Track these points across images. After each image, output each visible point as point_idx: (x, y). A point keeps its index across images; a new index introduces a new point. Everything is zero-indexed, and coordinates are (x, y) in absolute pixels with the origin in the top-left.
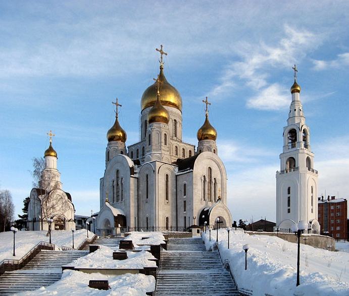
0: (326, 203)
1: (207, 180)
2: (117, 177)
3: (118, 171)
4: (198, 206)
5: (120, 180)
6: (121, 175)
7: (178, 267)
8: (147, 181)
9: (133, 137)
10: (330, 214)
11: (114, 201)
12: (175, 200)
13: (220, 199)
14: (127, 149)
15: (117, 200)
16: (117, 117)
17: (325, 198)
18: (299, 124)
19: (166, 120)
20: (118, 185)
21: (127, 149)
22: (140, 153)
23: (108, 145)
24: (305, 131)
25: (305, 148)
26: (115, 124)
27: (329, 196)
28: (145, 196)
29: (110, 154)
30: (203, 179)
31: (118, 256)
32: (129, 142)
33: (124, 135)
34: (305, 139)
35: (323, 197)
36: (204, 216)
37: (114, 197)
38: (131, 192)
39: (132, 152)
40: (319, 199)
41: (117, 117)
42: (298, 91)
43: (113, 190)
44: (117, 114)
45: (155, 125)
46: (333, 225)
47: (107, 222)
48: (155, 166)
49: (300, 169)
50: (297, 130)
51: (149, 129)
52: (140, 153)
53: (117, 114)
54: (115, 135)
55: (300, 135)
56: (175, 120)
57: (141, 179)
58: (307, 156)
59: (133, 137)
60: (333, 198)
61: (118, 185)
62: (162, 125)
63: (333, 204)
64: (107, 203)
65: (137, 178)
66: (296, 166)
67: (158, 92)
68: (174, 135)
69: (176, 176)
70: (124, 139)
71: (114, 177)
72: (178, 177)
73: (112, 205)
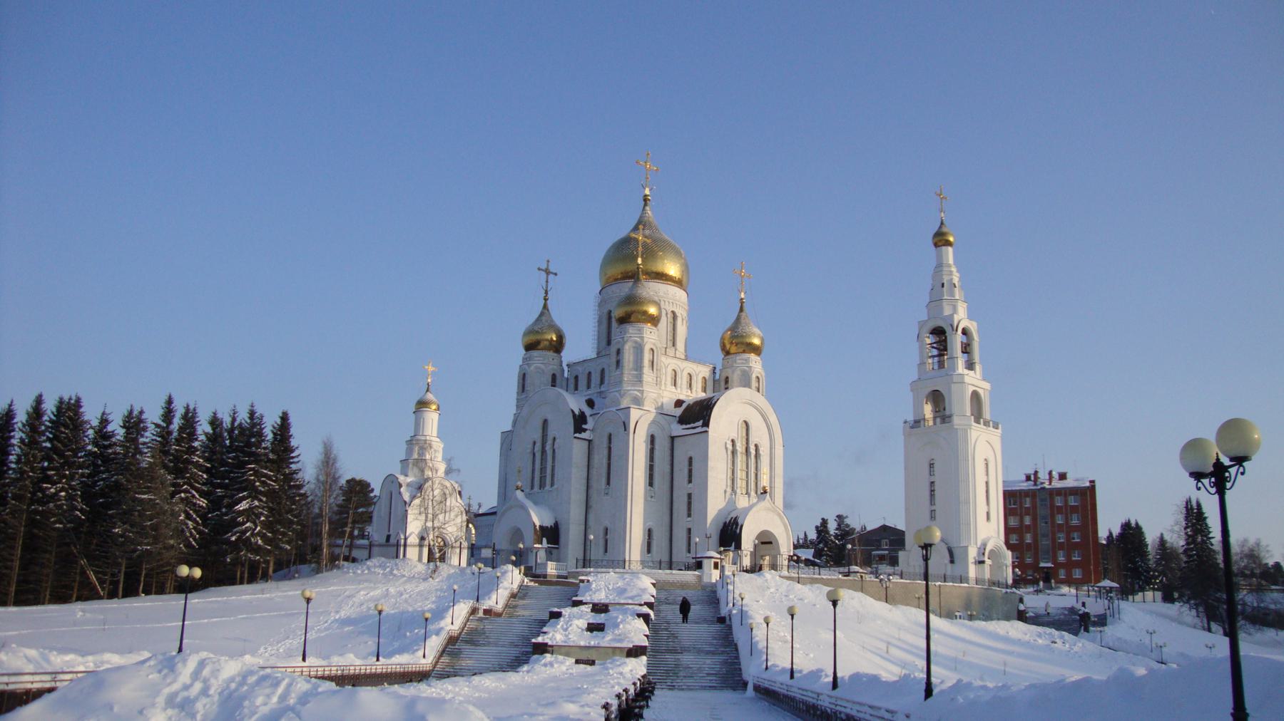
0: (1043, 488)
1: (740, 448)
2: (544, 436)
3: (545, 422)
4: (715, 505)
5: (549, 442)
6: (551, 433)
7: (24, 567)
8: (610, 448)
9: (581, 346)
10: (1053, 516)
11: (532, 487)
12: (668, 512)
13: (765, 492)
14: (566, 369)
15: (542, 486)
16: (546, 300)
17: (1043, 476)
18: (952, 316)
19: (654, 320)
20: (543, 451)
21: (566, 369)
22: (595, 378)
23: (525, 359)
24: (965, 332)
25: (966, 372)
26: (542, 314)
27: (1050, 473)
28: (604, 480)
29: (528, 381)
30: (730, 447)
31: (592, 628)
32: (572, 353)
33: (561, 338)
34: (966, 349)
35: (1036, 473)
36: (729, 535)
37: (533, 478)
38: (574, 470)
39: (576, 377)
40: (1028, 478)
41: (546, 300)
42: (948, 244)
43: (531, 462)
44: (546, 292)
45: (631, 330)
46: (1061, 546)
47: (517, 535)
48: (628, 416)
49: (956, 420)
50: (948, 330)
51: (615, 338)
52: (595, 378)
53: (546, 292)
54: (542, 340)
55: (957, 341)
56: (673, 312)
57: (596, 442)
58: (971, 389)
59: (581, 346)
60: (1063, 476)
61: (543, 451)
62: (648, 327)
63: (1059, 492)
64: (519, 494)
65: (590, 441)
66: (947, 413)
67: (640, 261)
68: (670, 344)
69: (673, 438)
70: (558, 347)
71: (537, 436)
72: (677, 442)
73: (528, 496)
